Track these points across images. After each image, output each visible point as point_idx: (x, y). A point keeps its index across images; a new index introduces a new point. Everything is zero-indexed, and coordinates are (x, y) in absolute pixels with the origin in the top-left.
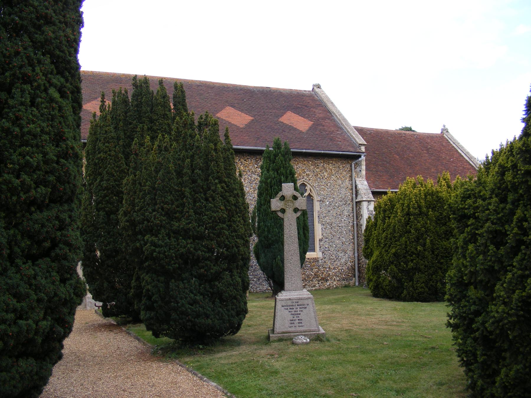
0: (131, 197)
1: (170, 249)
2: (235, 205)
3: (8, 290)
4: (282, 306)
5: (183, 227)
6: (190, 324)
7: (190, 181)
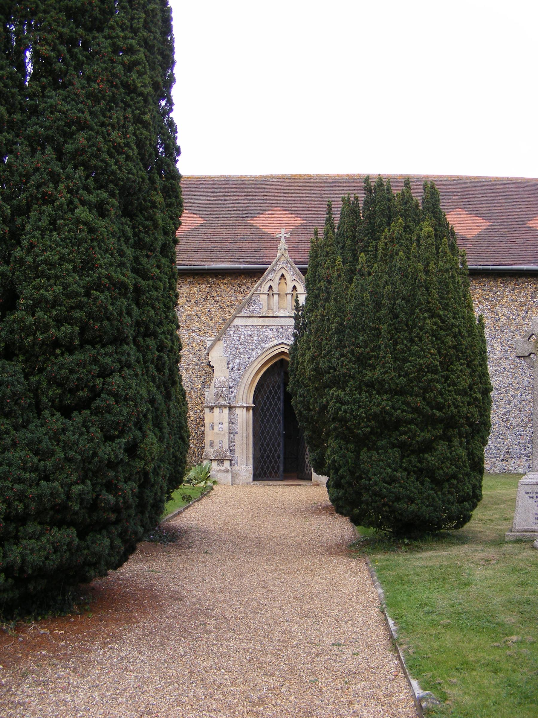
0: (318, 337)
1: (360, 407)
2: (455, 347)
3: (27, 445)
4: (526, 493)
5: (377, 378)
6: (388, 509)
7: (391, 315)
